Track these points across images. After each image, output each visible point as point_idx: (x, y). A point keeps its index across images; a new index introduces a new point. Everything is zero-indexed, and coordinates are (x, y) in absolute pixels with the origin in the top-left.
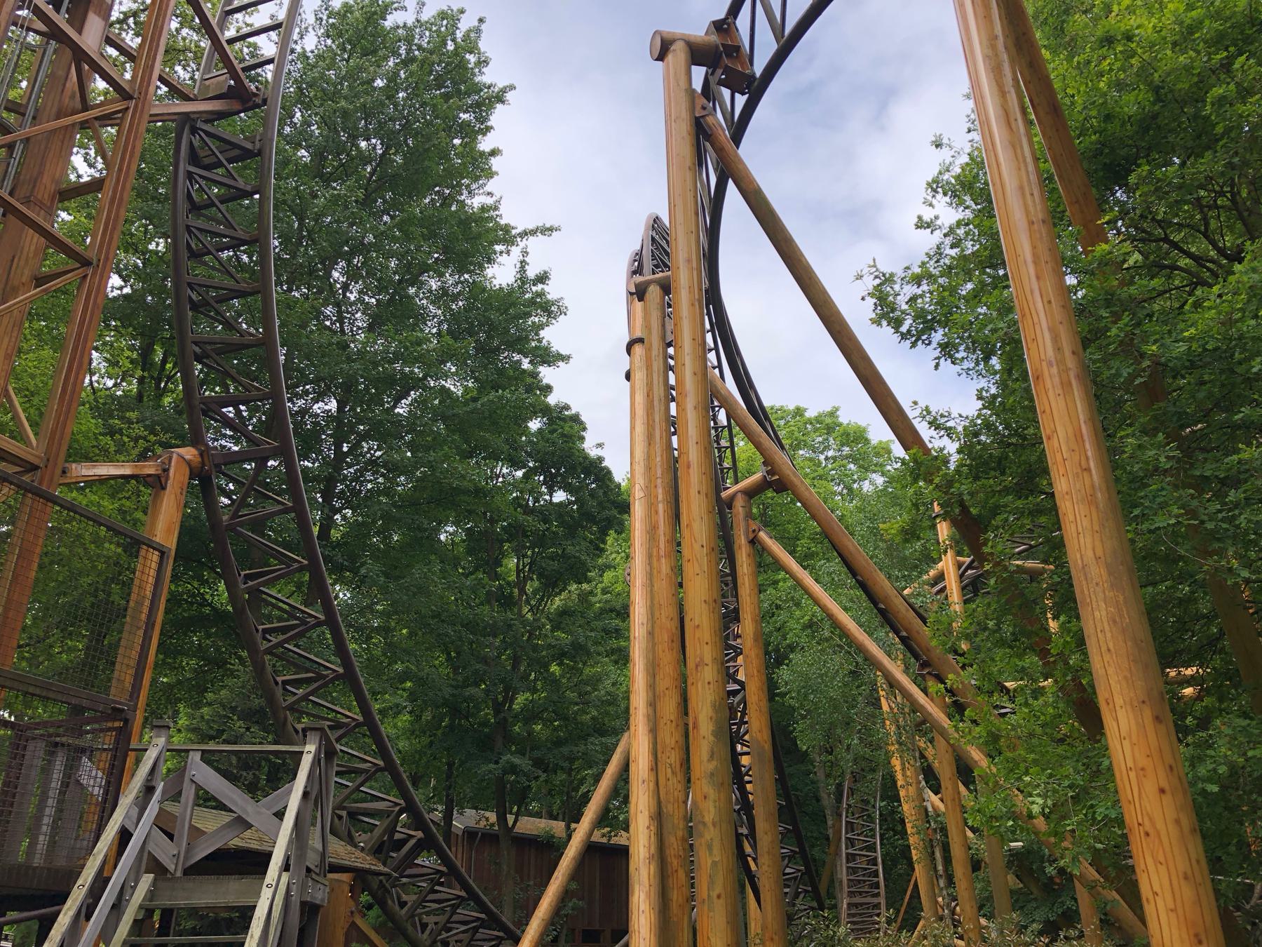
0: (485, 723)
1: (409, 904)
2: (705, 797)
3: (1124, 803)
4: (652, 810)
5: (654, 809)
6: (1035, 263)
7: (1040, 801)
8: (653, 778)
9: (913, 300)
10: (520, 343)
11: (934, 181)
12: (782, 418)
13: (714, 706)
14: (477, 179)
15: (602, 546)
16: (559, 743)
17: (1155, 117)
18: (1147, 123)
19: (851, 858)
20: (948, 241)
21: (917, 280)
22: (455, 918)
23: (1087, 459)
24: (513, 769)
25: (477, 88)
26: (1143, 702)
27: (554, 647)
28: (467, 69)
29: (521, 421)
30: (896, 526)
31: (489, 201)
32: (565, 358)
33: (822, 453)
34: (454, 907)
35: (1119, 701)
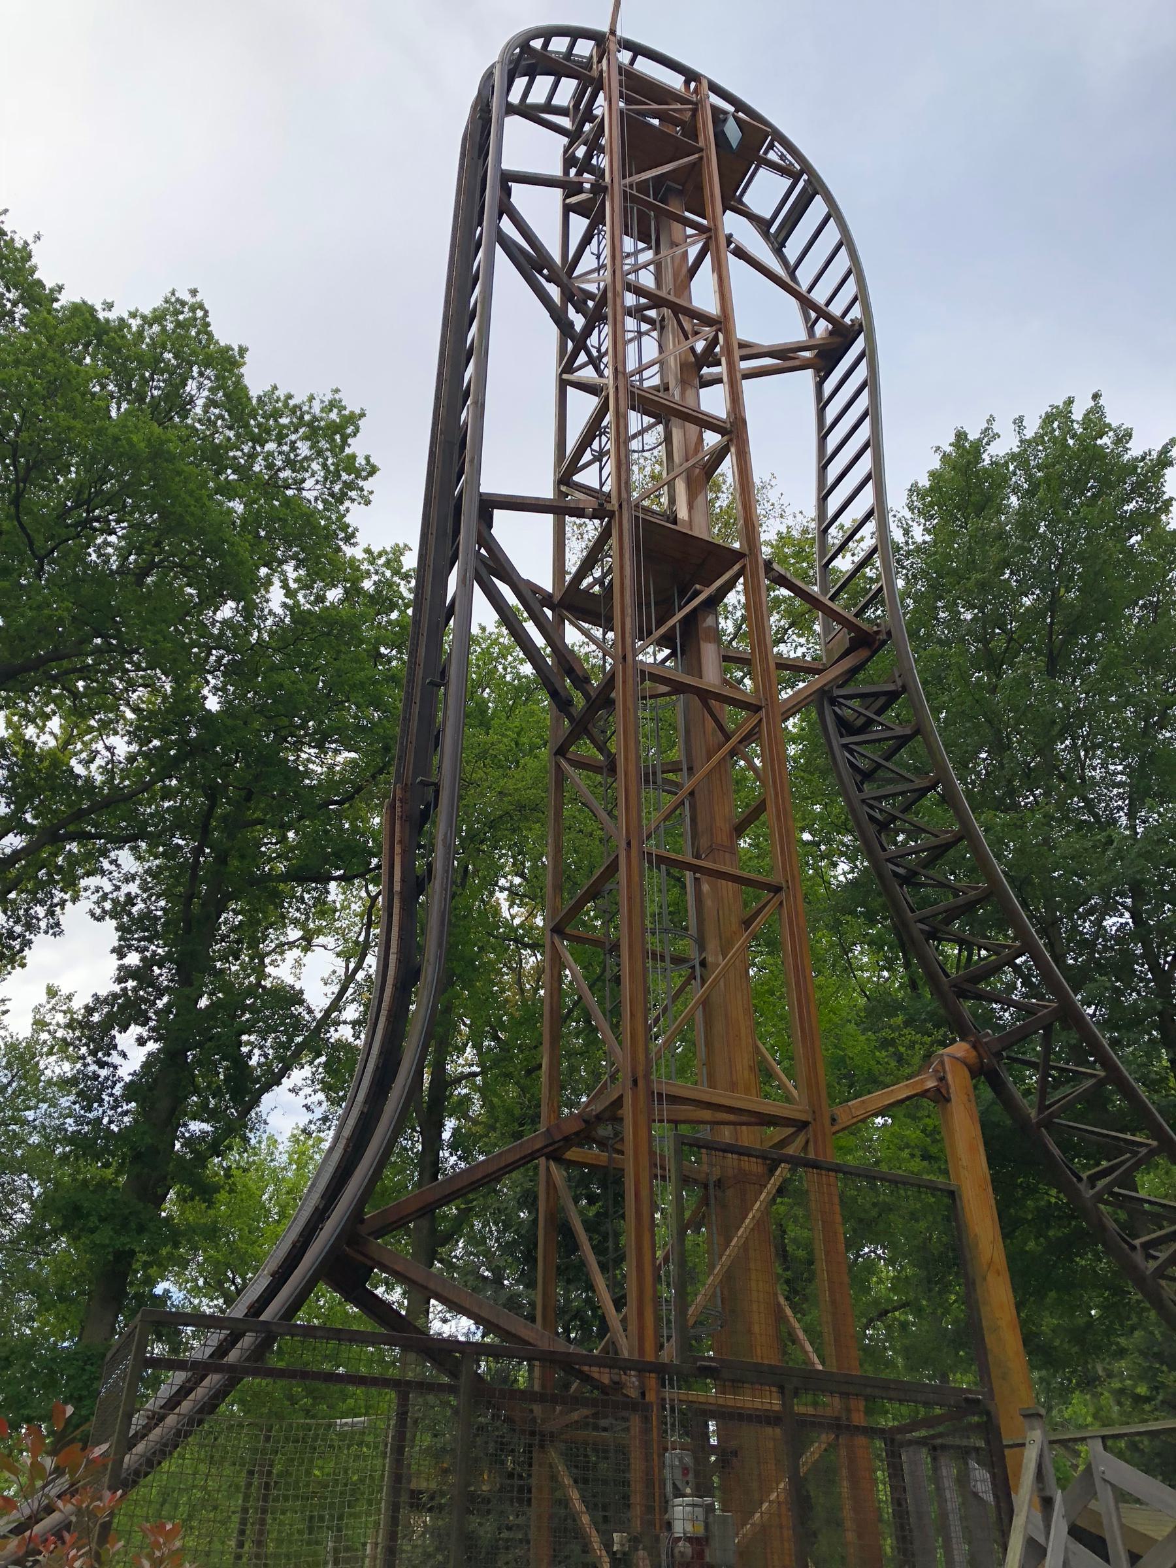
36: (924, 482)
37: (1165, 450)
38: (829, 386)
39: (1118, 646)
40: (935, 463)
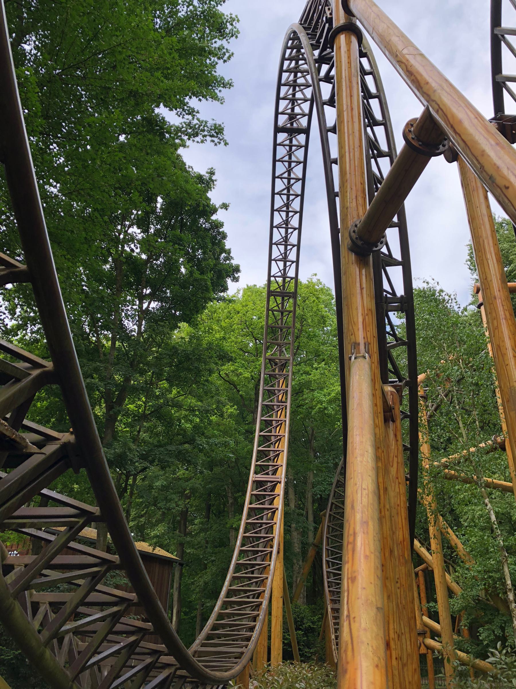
1: (17, 569)
22: (93, 597)
34: (96, 578)
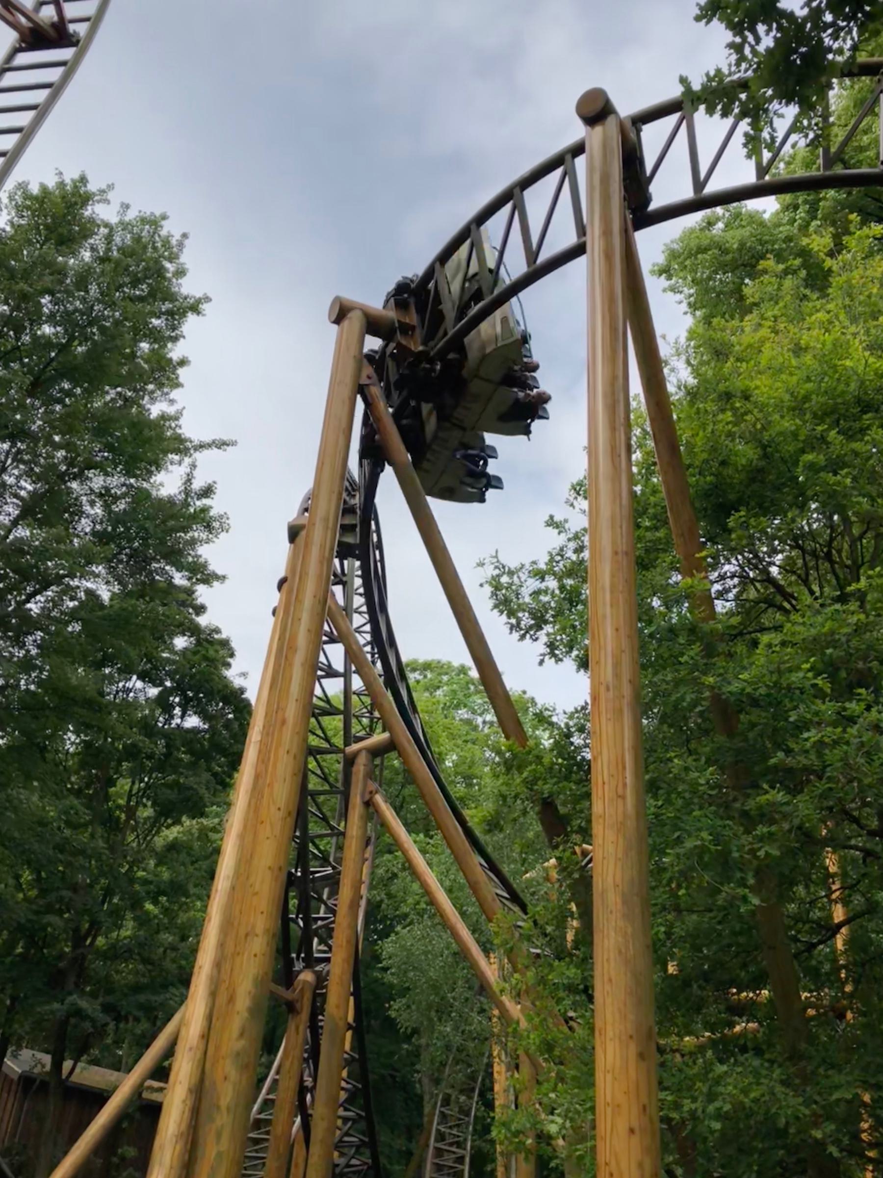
0: (61, 956)
2: (226, 1078)
3: (598, 1138)
4: (193, 1081)
5: (195, 1080)
6: (612, 592)
7: (559, 1120)
8: (202, 1047)
9: (536, 593)
10: (175, 556)
11: (578, 484)
12: (446, 674)
13: (255, 980)
14: (161, 386)
15: (228, 780)
16: (137, 989)
17: (760, 470)
18: (756, 475)
19: (439, 1152)
20: (572, 545)
21: (541, 575)
23: (625, 785)
24: (78, 1013)
25: (170, 297)
26: (631, 1037)
27: (151, 882)
28: (164, 278)
29: (162, 637)
30: (480, 815)
31: (171, 410)
32: (222, 578)
33: (481, 715)
35: (610, 1034)
36: (35, 189)
37: (199, 301)
38: (23, 58)
39: (86, 405)
40: (51, 183)
